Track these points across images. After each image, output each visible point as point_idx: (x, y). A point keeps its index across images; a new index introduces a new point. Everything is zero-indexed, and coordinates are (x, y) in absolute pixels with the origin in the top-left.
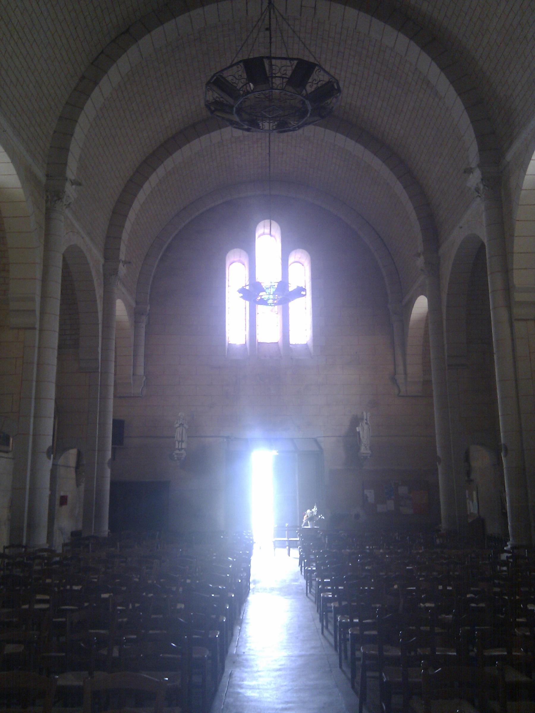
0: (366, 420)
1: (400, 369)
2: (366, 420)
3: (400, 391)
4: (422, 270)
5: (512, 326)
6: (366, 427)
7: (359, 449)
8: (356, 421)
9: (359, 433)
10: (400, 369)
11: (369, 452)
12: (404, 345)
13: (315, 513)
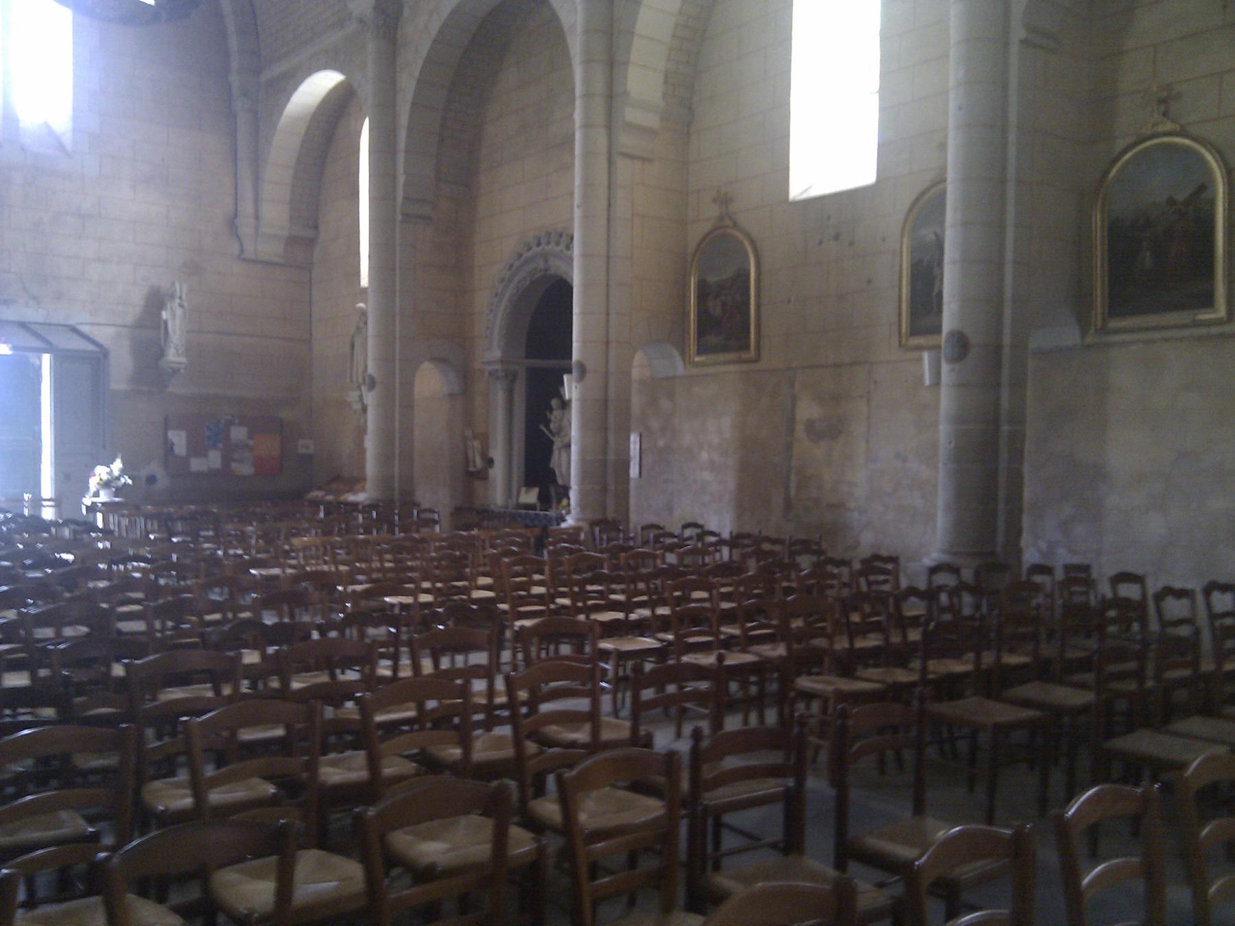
0: (180, 298)
1: (247, 208)
2: (180, 298)
3: (242, 251)
4: (361, 21)
5: (610, 162)
6: (179, 311)
7: (162, 353)
8: (156, 301)
9: (166, 323)
10: (247, 208)
11: (183, 360)
12: (257, 161)
13: (116, 473)
